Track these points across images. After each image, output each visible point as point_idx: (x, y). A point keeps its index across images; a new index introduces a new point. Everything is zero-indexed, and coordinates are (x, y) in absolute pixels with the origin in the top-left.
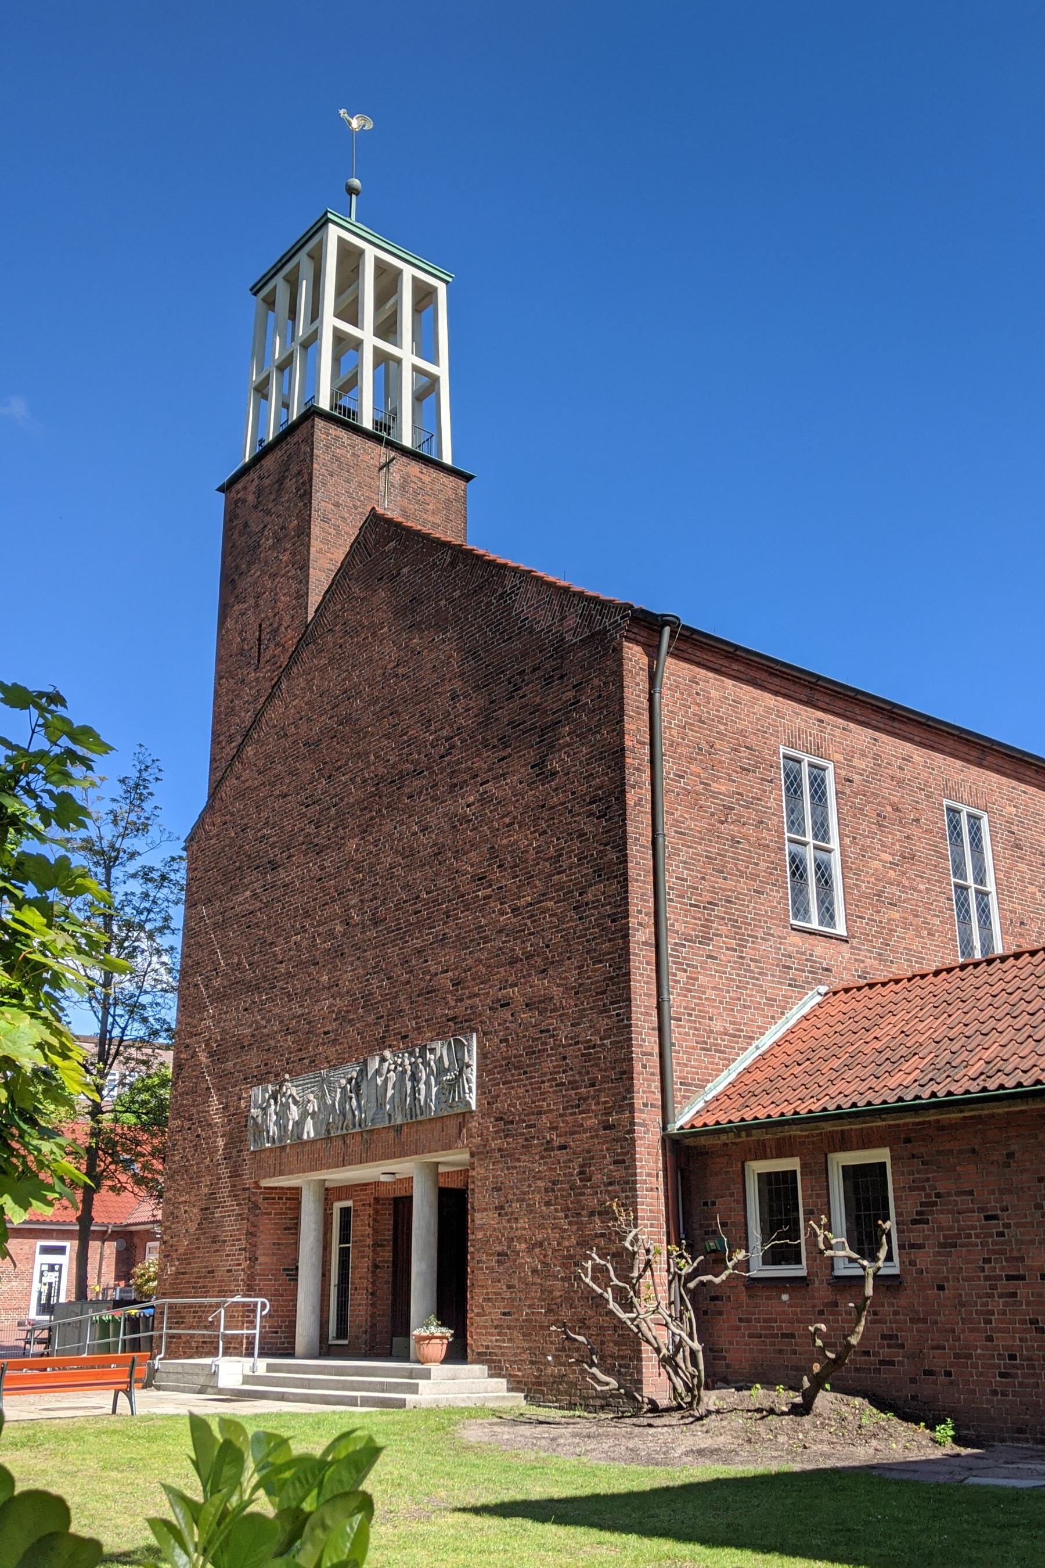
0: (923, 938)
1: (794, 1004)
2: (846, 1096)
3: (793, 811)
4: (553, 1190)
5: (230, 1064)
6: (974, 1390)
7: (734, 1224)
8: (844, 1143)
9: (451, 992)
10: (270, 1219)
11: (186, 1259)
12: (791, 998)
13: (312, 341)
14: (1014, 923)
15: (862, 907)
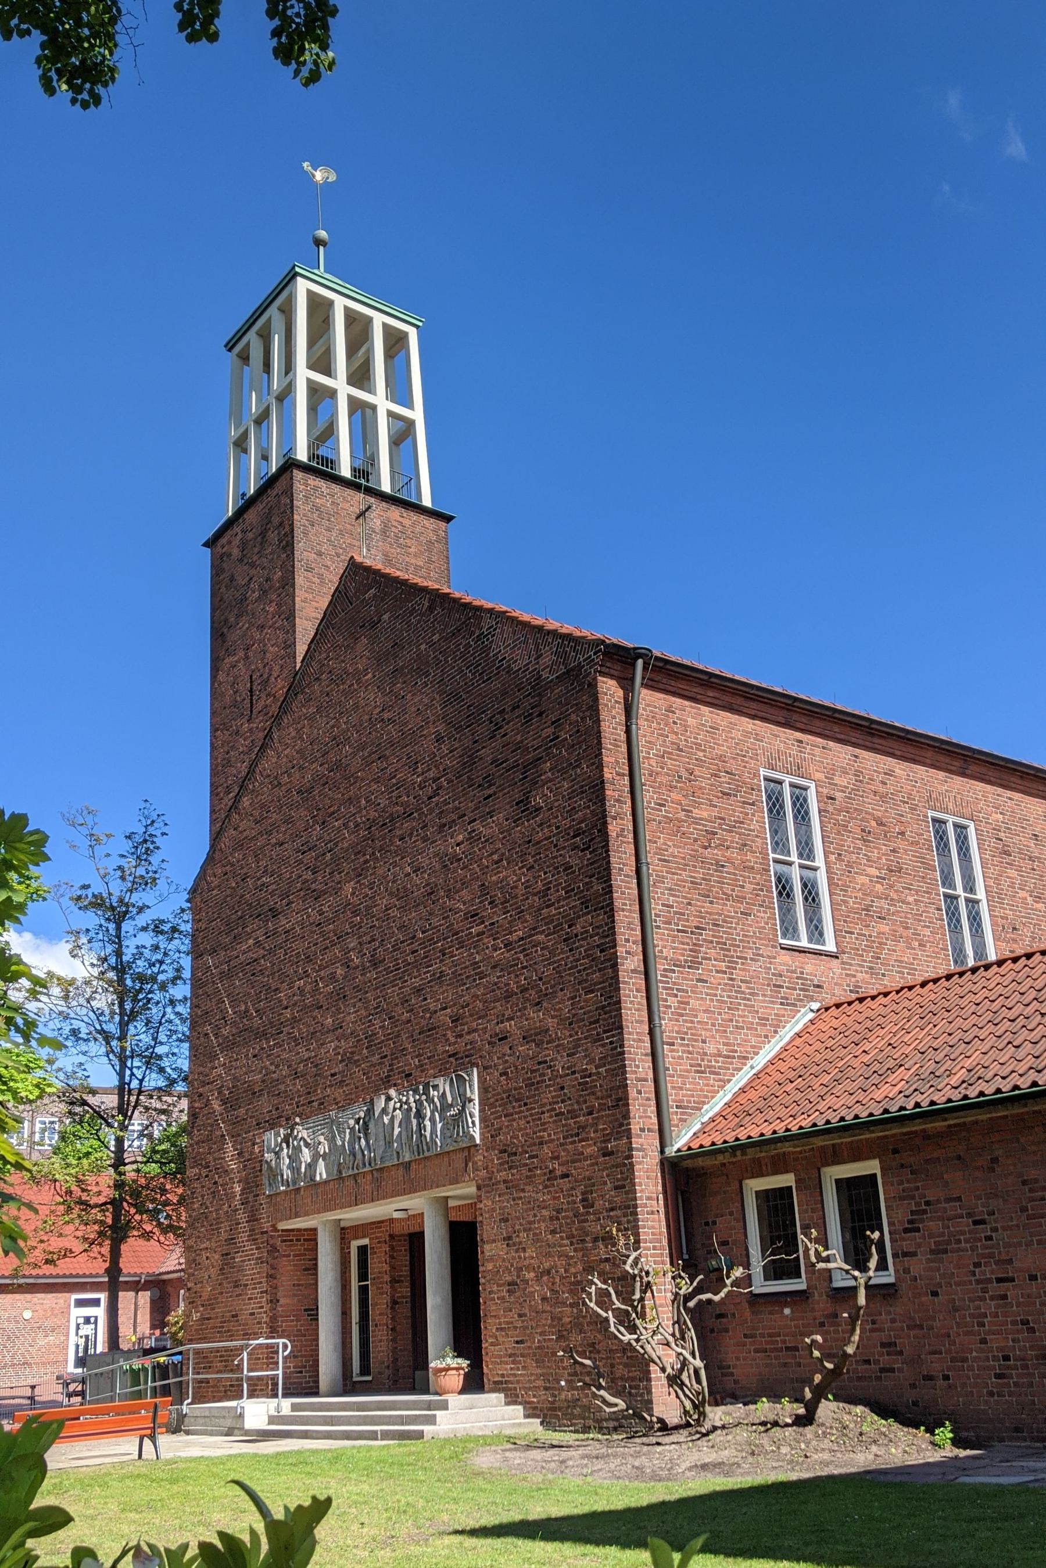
0: (914, 949)
1: (787, 1022)
2: (835, 1111)
3: (776, 832)
4: (558, 1219)
5: (242, 1111)
6: (972, 1392)
7: (735, 1242)
8: (836, 1157)
9: (451, 1028)
10: (289, 1261)
11: (210, 1305)
12: (783, 1016)
13: (286, 394)
14: (1006, 929)
15: (851, 922)
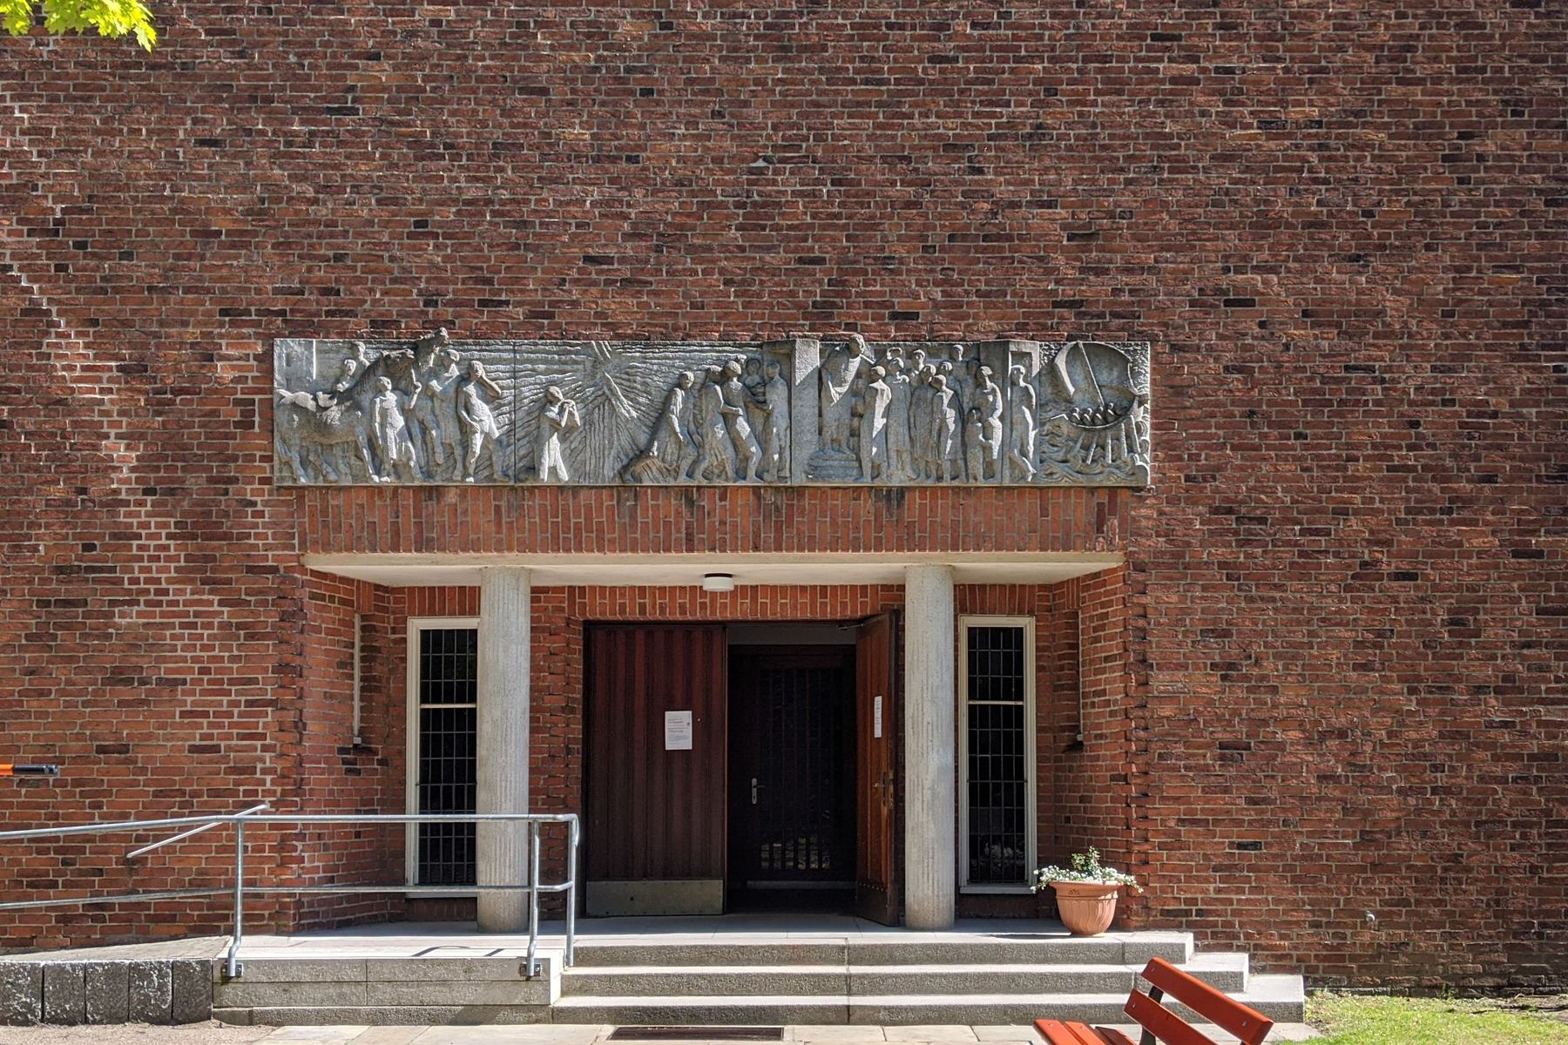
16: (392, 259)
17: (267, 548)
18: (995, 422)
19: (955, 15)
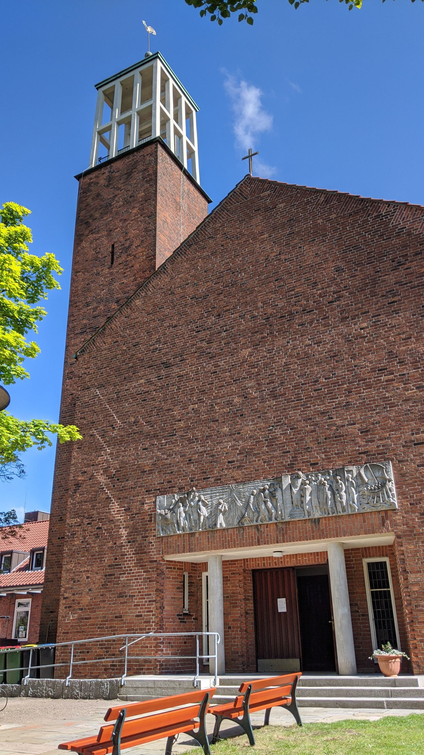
10: (170, 582)
16: (183, 471)
17: (155, 555)
18: (343, 493)
19: (320, 377)
